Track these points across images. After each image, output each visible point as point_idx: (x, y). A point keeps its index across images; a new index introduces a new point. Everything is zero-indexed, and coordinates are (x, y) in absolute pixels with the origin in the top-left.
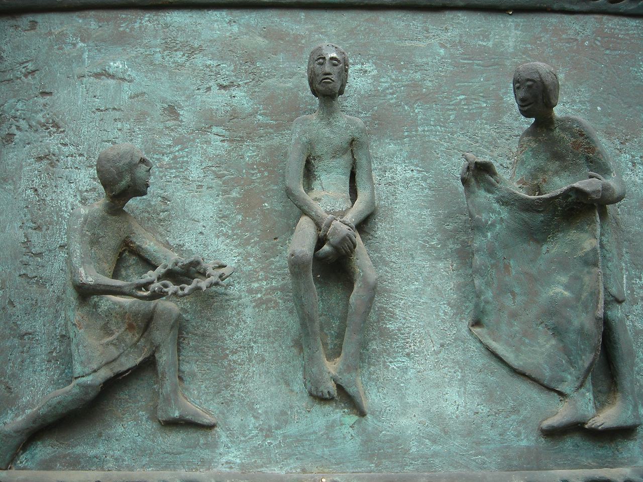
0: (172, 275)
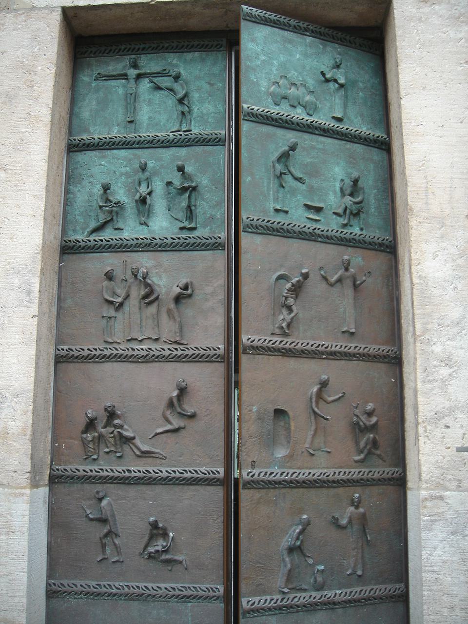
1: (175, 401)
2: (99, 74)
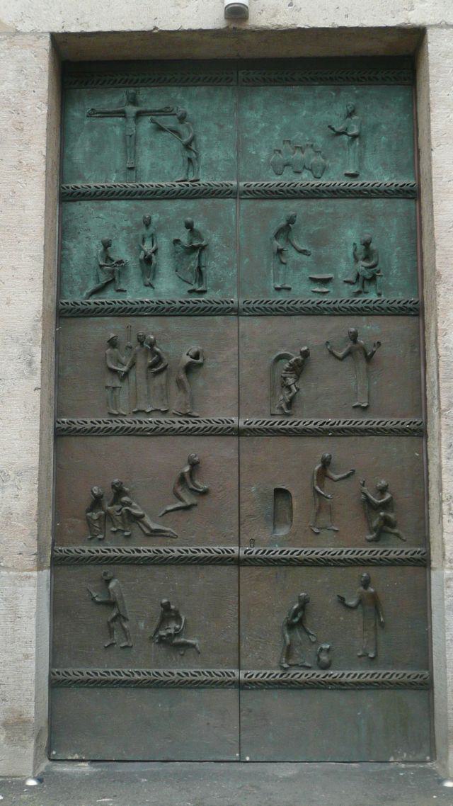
0: (117, 263)
1: (187, 476)
2: (92, 109)
